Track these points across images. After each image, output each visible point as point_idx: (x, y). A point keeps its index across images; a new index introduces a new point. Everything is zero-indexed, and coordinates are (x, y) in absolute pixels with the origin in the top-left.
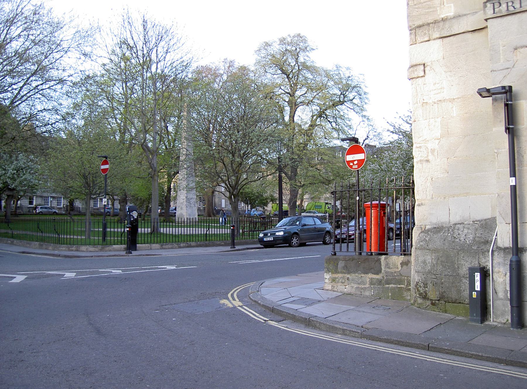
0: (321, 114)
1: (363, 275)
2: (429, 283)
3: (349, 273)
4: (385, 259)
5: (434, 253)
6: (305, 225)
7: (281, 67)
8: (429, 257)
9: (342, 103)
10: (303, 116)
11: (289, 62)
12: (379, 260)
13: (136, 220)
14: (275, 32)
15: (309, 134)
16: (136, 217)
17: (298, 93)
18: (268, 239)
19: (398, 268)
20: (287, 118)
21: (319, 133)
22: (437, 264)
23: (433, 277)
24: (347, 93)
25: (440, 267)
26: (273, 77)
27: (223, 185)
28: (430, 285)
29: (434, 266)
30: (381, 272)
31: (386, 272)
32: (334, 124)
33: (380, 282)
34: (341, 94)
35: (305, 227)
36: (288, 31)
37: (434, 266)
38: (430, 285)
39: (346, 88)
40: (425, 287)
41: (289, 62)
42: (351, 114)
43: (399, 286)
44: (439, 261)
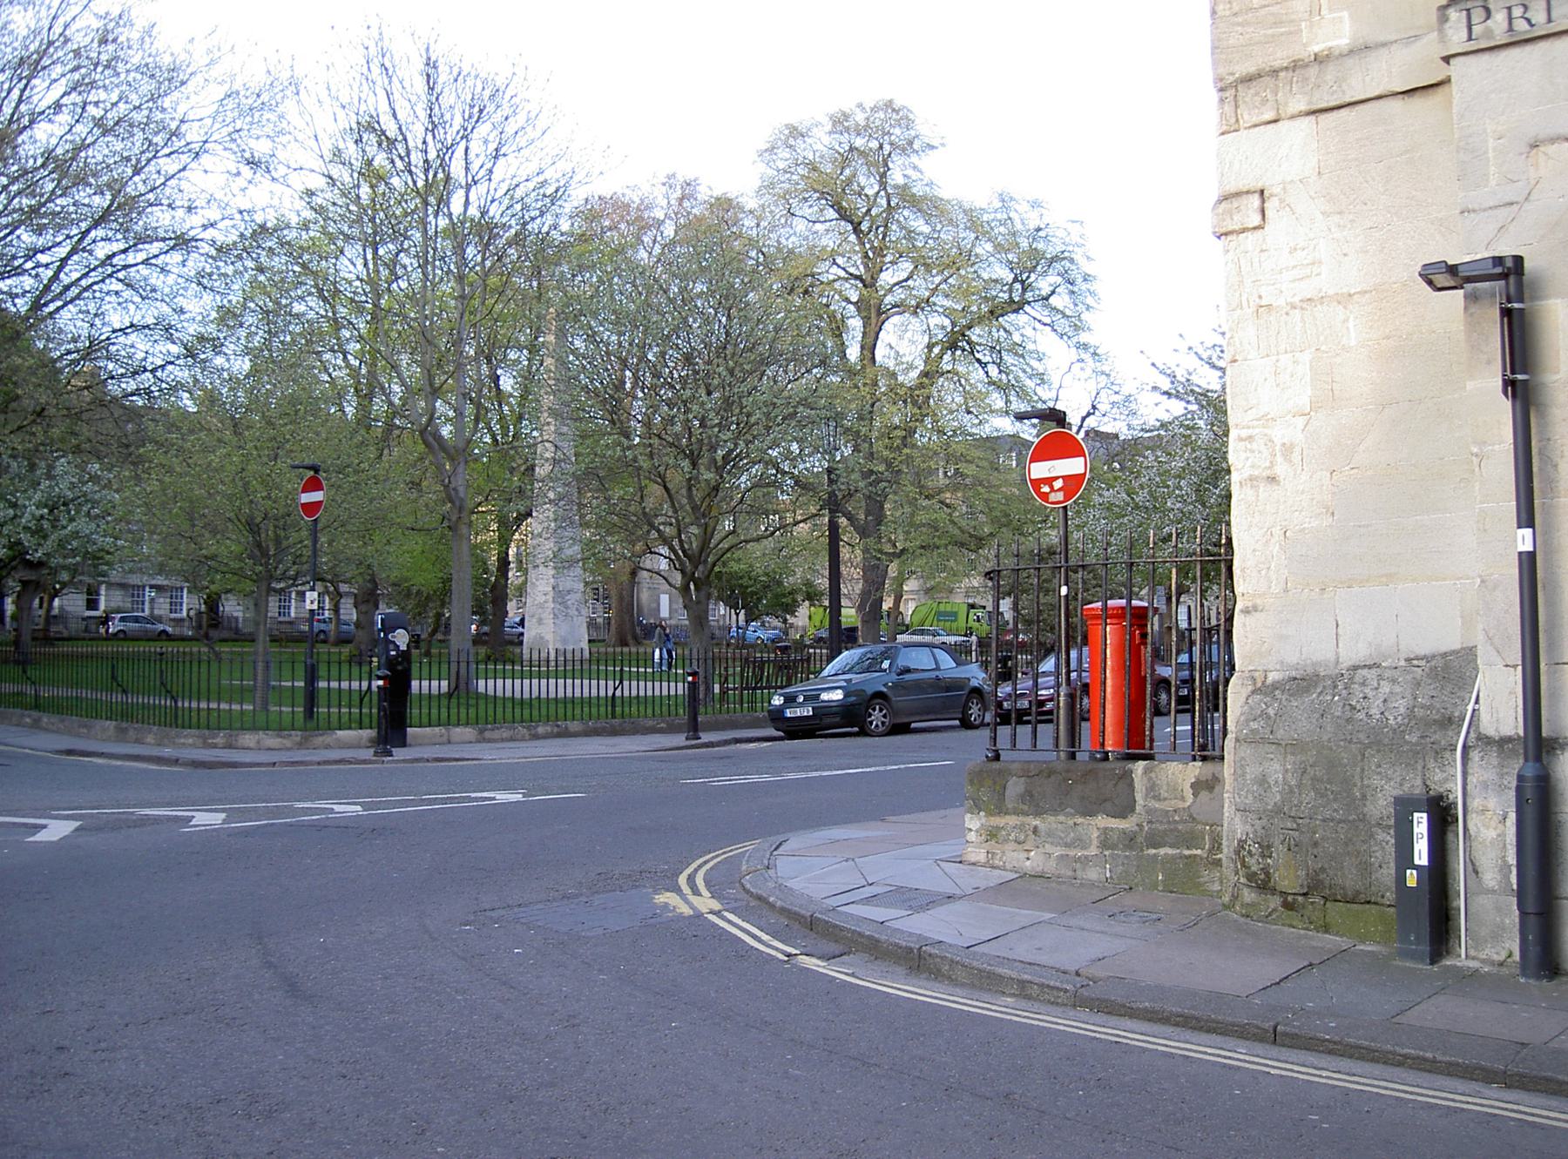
0: (955, 341)
1: (1080, 820)
2: (1277, 842)
3: (1037, 814)
4: (1146, 771)
5: (1293, 754)
6: (908, 671)
7: (837, 199)
8: (1277, 766)
9: (1017, 307)
10: (903, 345)
11: (860, 184)
12: (1127, 776)
13: (406, 656)
14: (819, 94)
15: (918, 398)
16: (403, 647)
17: (887, 278)
18: (799, 712)
19: (1183, 799)
20: (853, 353)
21: (948, 395)
22: (1299, 786)
23: (1289, 825)
24: (1033, 277)
25: (1309, 797)
26: (811, 230)
27: (664, 550)
28: (1279, 851)
29: (1291, 791)
30: (1133, 810)
31: (1149, 811)
32: (993, 371)
33: (1130, 840)
34: (1016, 280)
35: (907, 677)
36: (857, 92)
37: (1291, 791)
38: (1279, 851)
39: (1030, 262)
40: (1263, 856)
41: (860, 184)
42: (1046, 341)
43: (1187, 852)
44: (1306, 776)
